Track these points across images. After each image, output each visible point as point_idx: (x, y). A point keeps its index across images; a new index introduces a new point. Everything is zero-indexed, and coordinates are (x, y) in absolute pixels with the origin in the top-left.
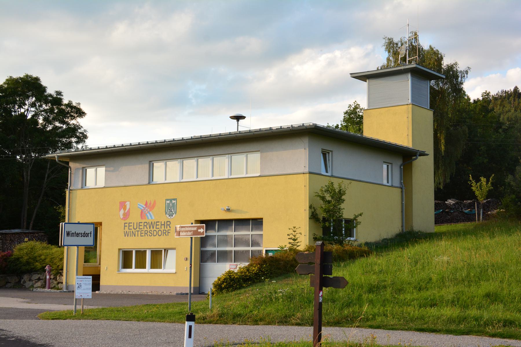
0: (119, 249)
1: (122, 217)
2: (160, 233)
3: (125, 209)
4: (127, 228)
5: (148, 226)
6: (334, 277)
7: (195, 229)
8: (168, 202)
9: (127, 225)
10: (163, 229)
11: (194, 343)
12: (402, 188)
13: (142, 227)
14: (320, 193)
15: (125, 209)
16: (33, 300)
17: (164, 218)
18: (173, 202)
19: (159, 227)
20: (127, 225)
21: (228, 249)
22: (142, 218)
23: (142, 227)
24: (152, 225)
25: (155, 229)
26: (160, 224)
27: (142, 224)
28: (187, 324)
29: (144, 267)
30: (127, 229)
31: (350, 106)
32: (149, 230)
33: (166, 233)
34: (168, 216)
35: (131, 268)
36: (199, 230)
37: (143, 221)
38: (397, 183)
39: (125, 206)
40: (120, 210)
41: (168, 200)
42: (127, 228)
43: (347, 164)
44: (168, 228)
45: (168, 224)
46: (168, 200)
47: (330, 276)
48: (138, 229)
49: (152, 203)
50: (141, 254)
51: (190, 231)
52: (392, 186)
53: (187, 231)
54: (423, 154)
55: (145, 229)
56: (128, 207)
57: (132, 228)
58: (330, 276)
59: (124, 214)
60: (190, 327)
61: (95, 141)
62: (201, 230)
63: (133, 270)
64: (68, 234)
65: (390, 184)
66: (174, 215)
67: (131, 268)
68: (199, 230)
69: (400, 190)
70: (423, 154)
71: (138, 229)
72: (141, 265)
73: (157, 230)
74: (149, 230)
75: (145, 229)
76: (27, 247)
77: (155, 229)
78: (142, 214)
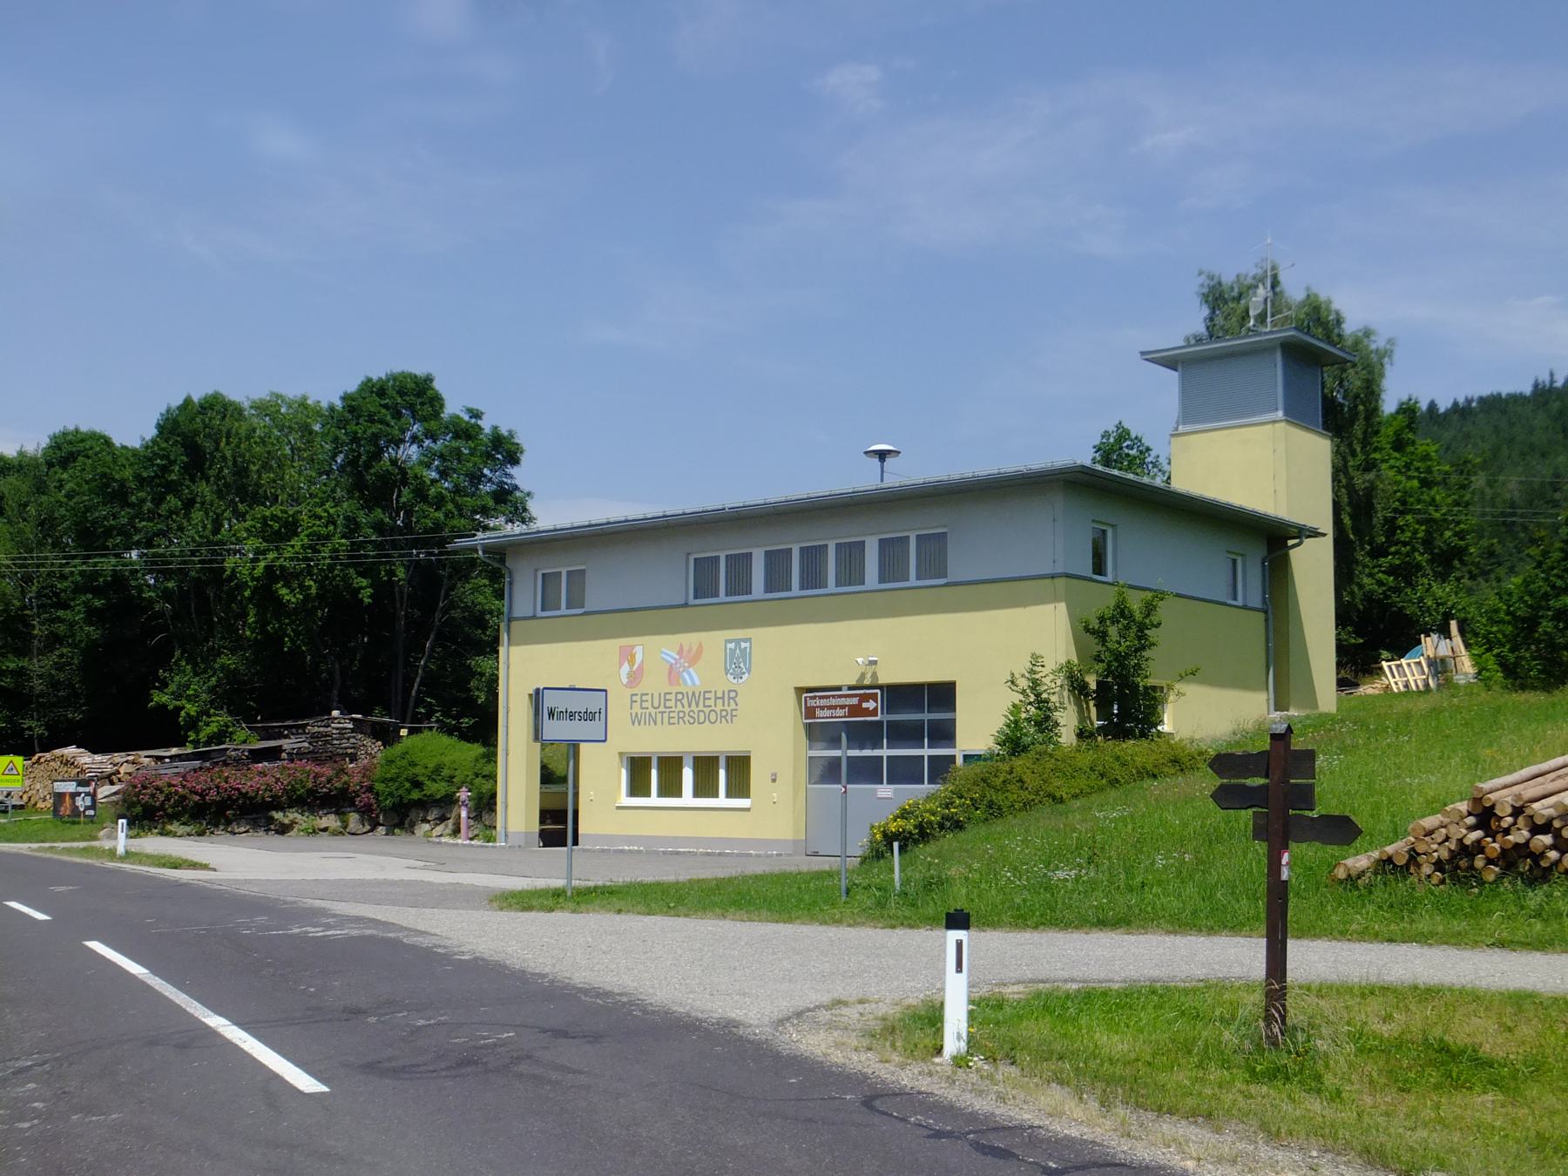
0: (621, 754)
1: (625, 681)
2: (713, 717)
3: (632, 663)
4: (637, 706)
5: (685, 701)
6: (1321, 816)
7: (855, 701)
8: (732, 646)
9: (637, 698)
10: (720, 707)
11: (971, 985)
12: (1266, 612)
13: (672, 704)
14: (1095, 624)
15: (632, 663)
16: (440, 865)
17: (726, 683)
18: (743, 645)
19: (711, 702)
20: (637, 698)
21: (876, 753)
22: (671, 683)
23: (672, 704)
24: (694, 698)
25: (701, 707)
26: (712, 695)
27: (672, 697)
28: (954, 935)
29: (679, 794)
30: (637, 708)
31: (1106, 435)
32: (687, 710)
33: (728, 716)
34: (730, 677)
35: (648, 795)
36: (865, 705)
37: (674, 689)
38: (1256, 601)
39: (633, 656)
40: (621, 665)
41: (731, 641)
42: (637, 706)
43: (1146, 560)
44: (733, 706)
45: (732, 695)
46: (731, 641)
47: (1309, 813)
48: (662, 709)
49: (695, 648)
50: (671, 766)
51: (842, 707)
52: (1245, 607)
53: (835, 707)
54: (1315, 533)
55: (680, 707)
56: (639, 658)
57: (648, 705)
58: (1309, 813)
59: (630, 675)
60: (959, 944)
61: (548, 515)
62: (871, 705)
63: (654, 800)
64: (551, 714)
65: (1240, 602)
66: (745, 677)
67: (648, 795)
68: (865, 705)
69: (1261, 616)
70: (1315, 533)
71: (662, 709)
72: (671, 787)
73: (707, 710)
74: (687, 710)
75: (680, 707)
76: (430, 747)
77: (701, 707)
78: (673, 675)
